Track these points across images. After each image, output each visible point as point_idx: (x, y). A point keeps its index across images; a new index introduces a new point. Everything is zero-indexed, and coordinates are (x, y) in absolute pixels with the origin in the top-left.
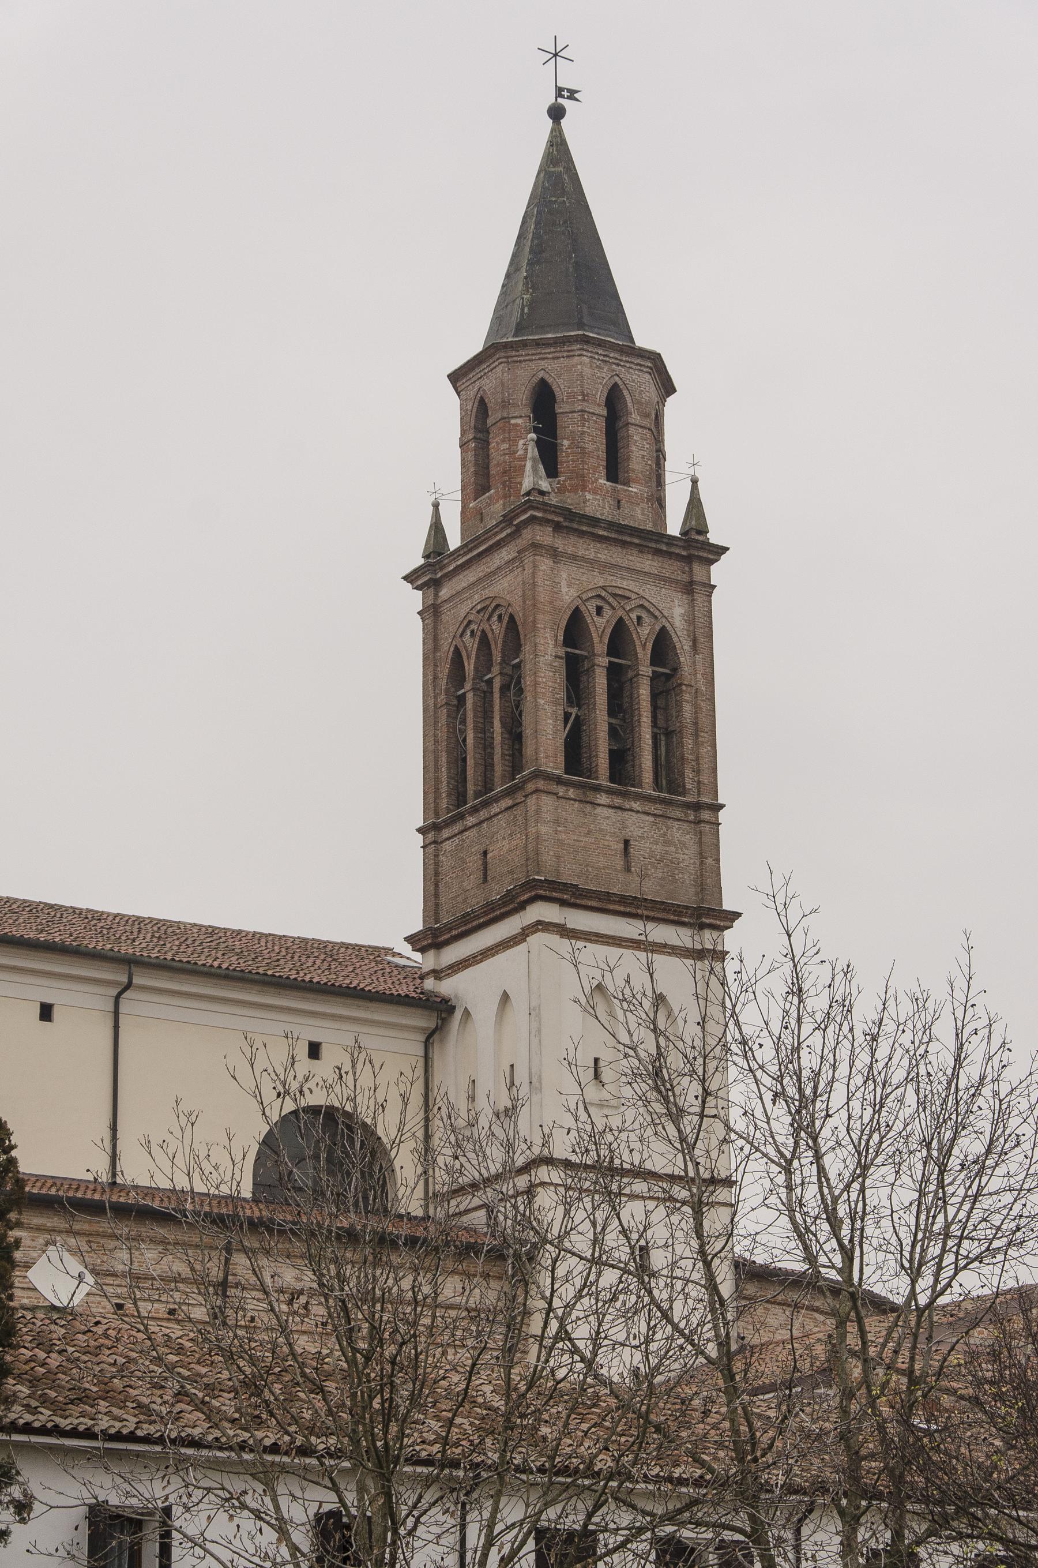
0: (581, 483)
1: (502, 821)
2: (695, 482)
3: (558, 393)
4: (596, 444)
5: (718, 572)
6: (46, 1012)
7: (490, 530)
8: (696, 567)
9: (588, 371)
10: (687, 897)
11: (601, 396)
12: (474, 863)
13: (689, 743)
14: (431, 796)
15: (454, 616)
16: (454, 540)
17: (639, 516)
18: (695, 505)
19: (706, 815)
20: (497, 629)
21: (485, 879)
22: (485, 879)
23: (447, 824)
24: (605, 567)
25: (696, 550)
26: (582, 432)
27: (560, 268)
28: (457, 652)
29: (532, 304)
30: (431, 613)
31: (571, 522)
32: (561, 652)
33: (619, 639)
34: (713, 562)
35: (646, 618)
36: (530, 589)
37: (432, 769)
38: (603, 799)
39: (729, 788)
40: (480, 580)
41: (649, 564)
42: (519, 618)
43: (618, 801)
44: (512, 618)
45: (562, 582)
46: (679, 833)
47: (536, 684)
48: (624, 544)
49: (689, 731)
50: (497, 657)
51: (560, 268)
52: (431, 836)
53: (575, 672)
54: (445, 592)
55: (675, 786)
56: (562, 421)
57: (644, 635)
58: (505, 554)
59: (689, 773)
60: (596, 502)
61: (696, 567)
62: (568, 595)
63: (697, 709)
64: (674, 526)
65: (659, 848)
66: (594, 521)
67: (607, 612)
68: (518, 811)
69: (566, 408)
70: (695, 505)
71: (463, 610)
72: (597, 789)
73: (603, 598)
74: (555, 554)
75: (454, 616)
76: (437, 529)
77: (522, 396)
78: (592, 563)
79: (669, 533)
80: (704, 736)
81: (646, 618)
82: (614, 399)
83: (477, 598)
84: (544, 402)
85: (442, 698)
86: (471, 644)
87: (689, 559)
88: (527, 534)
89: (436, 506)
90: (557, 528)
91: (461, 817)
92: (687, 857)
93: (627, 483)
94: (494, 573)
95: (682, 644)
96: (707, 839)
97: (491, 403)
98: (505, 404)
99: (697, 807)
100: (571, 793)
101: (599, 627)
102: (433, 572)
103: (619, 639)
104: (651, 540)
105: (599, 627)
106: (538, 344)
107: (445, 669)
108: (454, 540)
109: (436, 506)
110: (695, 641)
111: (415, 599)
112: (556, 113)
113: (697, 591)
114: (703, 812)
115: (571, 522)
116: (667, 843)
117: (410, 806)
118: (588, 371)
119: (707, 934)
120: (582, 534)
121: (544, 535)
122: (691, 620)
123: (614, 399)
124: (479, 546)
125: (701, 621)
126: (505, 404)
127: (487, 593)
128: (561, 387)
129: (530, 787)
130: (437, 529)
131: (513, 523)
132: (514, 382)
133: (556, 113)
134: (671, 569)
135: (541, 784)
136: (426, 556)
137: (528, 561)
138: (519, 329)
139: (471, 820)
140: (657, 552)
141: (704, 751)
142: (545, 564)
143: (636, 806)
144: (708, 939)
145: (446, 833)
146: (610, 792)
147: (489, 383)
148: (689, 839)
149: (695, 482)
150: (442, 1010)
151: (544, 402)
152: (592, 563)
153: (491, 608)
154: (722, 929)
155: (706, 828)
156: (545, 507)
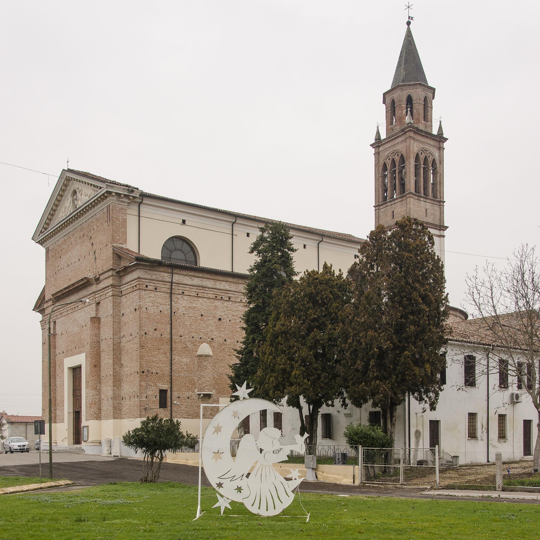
0: (418, 121)
1: (398, 204)
2: (440, 122)
3: (413, 98)
4: (422, 112)
5: (446, 145)
6: (305, 246)
7: (396, 134)
8: (441, 143)
9: (420, 93)
10: (437, 223)
11: (423, 99)
12: (390, 214)
13: (438, 186)
14: (377, 199)
15: (383, 155)
16: (383, 136)
17: (428, 130)
18: (440, 128)
19: (442, 204)
20: (397, 159)
21: (393, 218)
22: (393, 218)
23: (382, 205)
24: (424, 143)
25: (440, 139)
26: (418, 107)
27: (410, 63)
28: (385, 163)
29: (406, 75)
30: (377, 154)
31: (417, 131)
32: (415, 163)
33: (426, 159)
34: (444, 142)
35: (431, 156)
36: (408, 148)
37: (377, 191)
38: (422, 199)
39: (447, 197)
40: (392, 146)
41: (432, 142)
42: (405, 155)
43: (425, 200)
44: (402, 155)
45: (415, 146)
46: (436, 208)
47: (410, 171)
48: (427, 137)
49: (438, 184)
50: (397, 164)
51: (410, 63)
52: (377, 208)
53: (417, 167)
54: (381, 149)
55: (435, 196)
56: (414, 105)
57: (430, 159)
58: (400, 139)
59: (438, 194)
60: (421, 127)
61: (441, 143)
62: (416, 150)
63: (440, 177)
64: (435, 132)
65: (432, 211)
66: (422, 131)
67: (423, 154)
68: (403, 202)
69: (415, 102)
70: (440, 128)
71: (386, 154)
72: (421, 197)
73: (424, 150)
74: (414, 139)
75: (383, 155)
76: (378, 133)
77: (404, 99)
78: (421, 141)
79: (433, 133)
80: (442, 185)
81: (431, 156)
82: (425, 99)
83: (391, 150)
84: (409, 100)
85: (380, 175)
86: (389, 163)
87: (440, 141)
88: (408, 134)
89: (378, 127)
90: (415, 132)
91: (386, 203)
92: (438, 213)
93: (428, 122)
94: (397, 144)
95: (438, 162)
96: (442, 209)
97: (396, 101)
98: (400, 101)
99: (440, 202)
100: (416, 198)
101: (422, 157)
102: (378, 144)
103: (426, 159)
104: (429, 135)
105: (422, 157)
106: (409, 85)
107: (381, 168)
108: (383, 136)
109: (378, 127)
110: (440, 162)
111: (373, 150)
112: (409, 23)
113: (441, 149)
114: (441, 203)
115: (417, 131)
116: (434, 210)
117: (372, 202)
118: (420, 93)
119: (442, 231)
120: (419, 134)
121: (412, 134)
122: (440, 157)
123: (425, 99)
124: (391, 138)
125: (441, 157)
126: (400, 101)
127: (394, 149)
128: (414, 97)
129: (408, 196)
130: (378, 133)
131: (404, 131)
132: (401, 95)
133: (409, 23)
134: (436, 144)
135: (411, 195)
136: (376, 140)
137: (408, 140)
138: (403, 81)
139: (389, 204)
140: (433, 139)
141: (442, 188)
142: (412, 141)
143: (428, 201)
144: (442, 233)
145: (381, 207)
146: (424, 198)
147: (396, 95)
148: (438, 209)
149: (440, 122)
150: (444, 236)
151: (409, 100)
152: (421, 141)
153: (396, 153)
154: (444, 230)
155: (442, 207)
156: (413, 127)
